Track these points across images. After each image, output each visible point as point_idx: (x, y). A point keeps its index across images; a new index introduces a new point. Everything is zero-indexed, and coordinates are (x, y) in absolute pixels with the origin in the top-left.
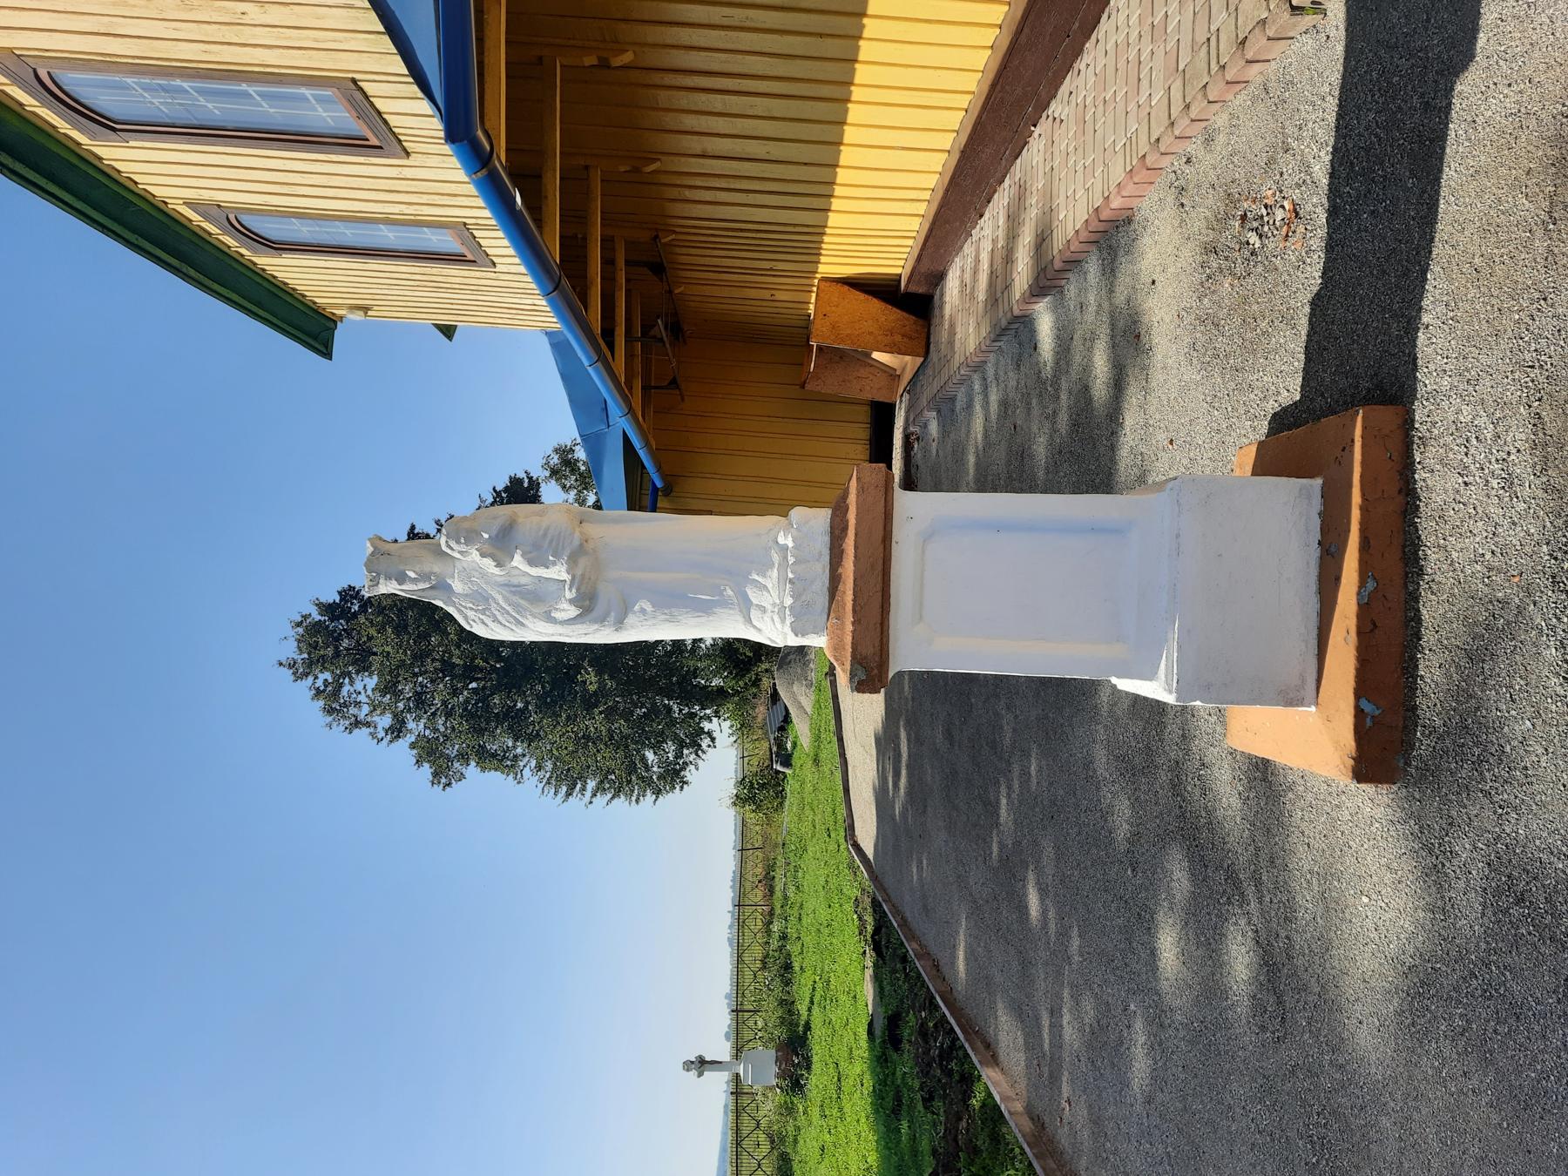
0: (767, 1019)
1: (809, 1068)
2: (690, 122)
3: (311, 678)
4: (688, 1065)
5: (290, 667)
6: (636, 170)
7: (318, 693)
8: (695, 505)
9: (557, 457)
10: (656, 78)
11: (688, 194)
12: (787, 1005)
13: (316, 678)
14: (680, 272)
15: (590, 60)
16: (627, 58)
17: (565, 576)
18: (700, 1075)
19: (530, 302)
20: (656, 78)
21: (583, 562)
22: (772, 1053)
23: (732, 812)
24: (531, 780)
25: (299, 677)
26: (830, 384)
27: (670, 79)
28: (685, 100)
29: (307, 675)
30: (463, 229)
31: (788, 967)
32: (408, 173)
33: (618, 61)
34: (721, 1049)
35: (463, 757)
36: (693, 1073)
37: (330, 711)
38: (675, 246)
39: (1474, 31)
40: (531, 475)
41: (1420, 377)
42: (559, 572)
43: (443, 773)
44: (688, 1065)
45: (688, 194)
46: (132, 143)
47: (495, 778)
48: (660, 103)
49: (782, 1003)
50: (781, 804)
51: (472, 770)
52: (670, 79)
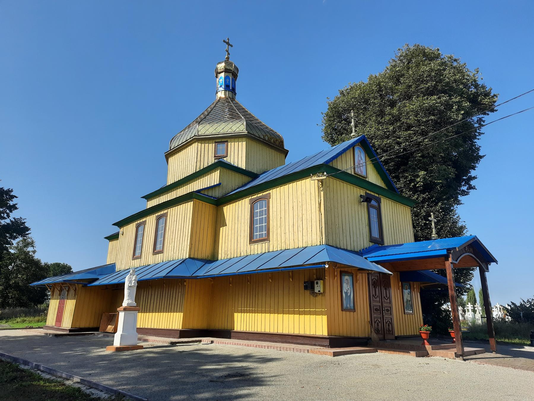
2: (156, 293)
6: (150, 285)
8: (138, 289)
9: (31, 241)
10: (162, 289)
11: (145, 292)
14: (160, 290)
15: (165, 282)
16: (165, 286)
17: (132, 285)
19: (124, 263)
20: (162, 289)
21: (133, 286)
26: (104, 318)
27: (148, 291)
28: (159, 292)
30: (140, 257)
32: (150, 254)
33: (164, 284)
38: (161, 289)
40: (29, 235)
42: (133, 284)
45: (145, 292)
46: (155, 221)
48: (452, 265)
52: (162, 290)
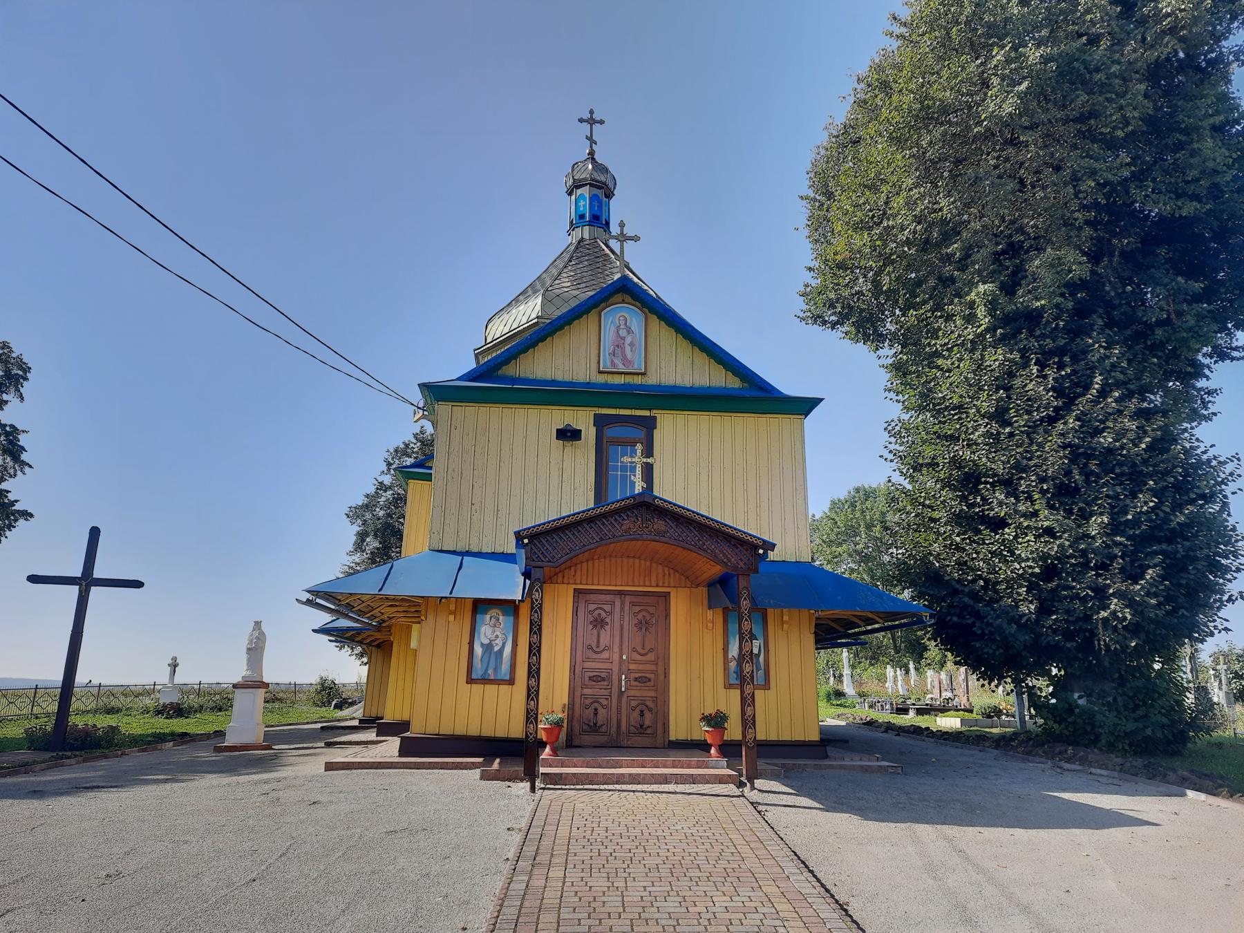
0: (193, 700)
1: (167, 718)
3: (415, 441)
4: (175, 659)
5: (421, 432)
7: (407, 446)
12: (201, 709)
13: (415, 444)
18: (169, 665)
22: (175, 700)
23: (314, 679)
24: (348, 560)
25: (415, 436)
29: (416, 439)
31: (220, 710)
34: (179, 679)
35: (365, 523)
36: (170, 662)
37: (396, 451)
39: (1108, 828)
41: (1214, 55)
43: (355, 514)
44: (175, 659)
47: (235, 682)
49: (201, 707)
50: (318, 706)
51: (356, 528)
